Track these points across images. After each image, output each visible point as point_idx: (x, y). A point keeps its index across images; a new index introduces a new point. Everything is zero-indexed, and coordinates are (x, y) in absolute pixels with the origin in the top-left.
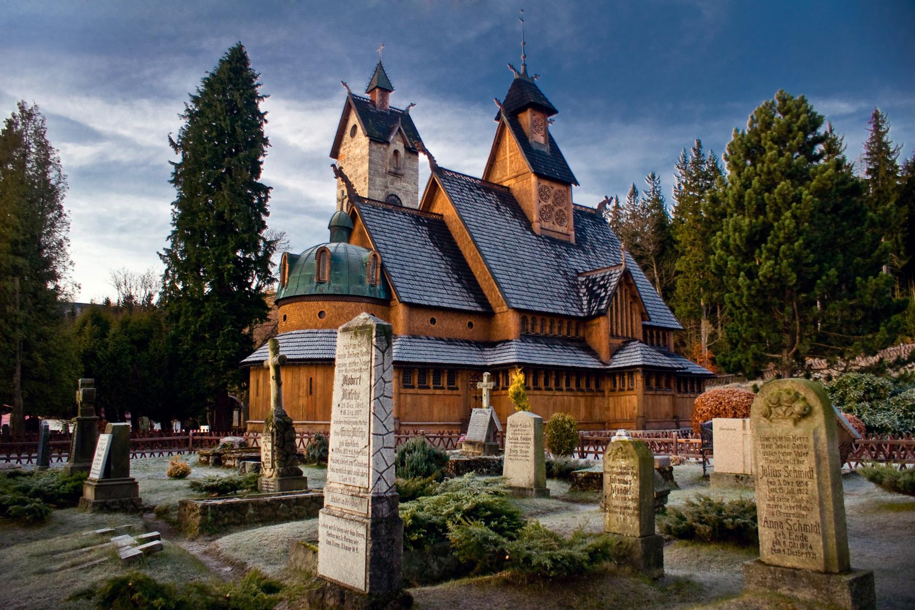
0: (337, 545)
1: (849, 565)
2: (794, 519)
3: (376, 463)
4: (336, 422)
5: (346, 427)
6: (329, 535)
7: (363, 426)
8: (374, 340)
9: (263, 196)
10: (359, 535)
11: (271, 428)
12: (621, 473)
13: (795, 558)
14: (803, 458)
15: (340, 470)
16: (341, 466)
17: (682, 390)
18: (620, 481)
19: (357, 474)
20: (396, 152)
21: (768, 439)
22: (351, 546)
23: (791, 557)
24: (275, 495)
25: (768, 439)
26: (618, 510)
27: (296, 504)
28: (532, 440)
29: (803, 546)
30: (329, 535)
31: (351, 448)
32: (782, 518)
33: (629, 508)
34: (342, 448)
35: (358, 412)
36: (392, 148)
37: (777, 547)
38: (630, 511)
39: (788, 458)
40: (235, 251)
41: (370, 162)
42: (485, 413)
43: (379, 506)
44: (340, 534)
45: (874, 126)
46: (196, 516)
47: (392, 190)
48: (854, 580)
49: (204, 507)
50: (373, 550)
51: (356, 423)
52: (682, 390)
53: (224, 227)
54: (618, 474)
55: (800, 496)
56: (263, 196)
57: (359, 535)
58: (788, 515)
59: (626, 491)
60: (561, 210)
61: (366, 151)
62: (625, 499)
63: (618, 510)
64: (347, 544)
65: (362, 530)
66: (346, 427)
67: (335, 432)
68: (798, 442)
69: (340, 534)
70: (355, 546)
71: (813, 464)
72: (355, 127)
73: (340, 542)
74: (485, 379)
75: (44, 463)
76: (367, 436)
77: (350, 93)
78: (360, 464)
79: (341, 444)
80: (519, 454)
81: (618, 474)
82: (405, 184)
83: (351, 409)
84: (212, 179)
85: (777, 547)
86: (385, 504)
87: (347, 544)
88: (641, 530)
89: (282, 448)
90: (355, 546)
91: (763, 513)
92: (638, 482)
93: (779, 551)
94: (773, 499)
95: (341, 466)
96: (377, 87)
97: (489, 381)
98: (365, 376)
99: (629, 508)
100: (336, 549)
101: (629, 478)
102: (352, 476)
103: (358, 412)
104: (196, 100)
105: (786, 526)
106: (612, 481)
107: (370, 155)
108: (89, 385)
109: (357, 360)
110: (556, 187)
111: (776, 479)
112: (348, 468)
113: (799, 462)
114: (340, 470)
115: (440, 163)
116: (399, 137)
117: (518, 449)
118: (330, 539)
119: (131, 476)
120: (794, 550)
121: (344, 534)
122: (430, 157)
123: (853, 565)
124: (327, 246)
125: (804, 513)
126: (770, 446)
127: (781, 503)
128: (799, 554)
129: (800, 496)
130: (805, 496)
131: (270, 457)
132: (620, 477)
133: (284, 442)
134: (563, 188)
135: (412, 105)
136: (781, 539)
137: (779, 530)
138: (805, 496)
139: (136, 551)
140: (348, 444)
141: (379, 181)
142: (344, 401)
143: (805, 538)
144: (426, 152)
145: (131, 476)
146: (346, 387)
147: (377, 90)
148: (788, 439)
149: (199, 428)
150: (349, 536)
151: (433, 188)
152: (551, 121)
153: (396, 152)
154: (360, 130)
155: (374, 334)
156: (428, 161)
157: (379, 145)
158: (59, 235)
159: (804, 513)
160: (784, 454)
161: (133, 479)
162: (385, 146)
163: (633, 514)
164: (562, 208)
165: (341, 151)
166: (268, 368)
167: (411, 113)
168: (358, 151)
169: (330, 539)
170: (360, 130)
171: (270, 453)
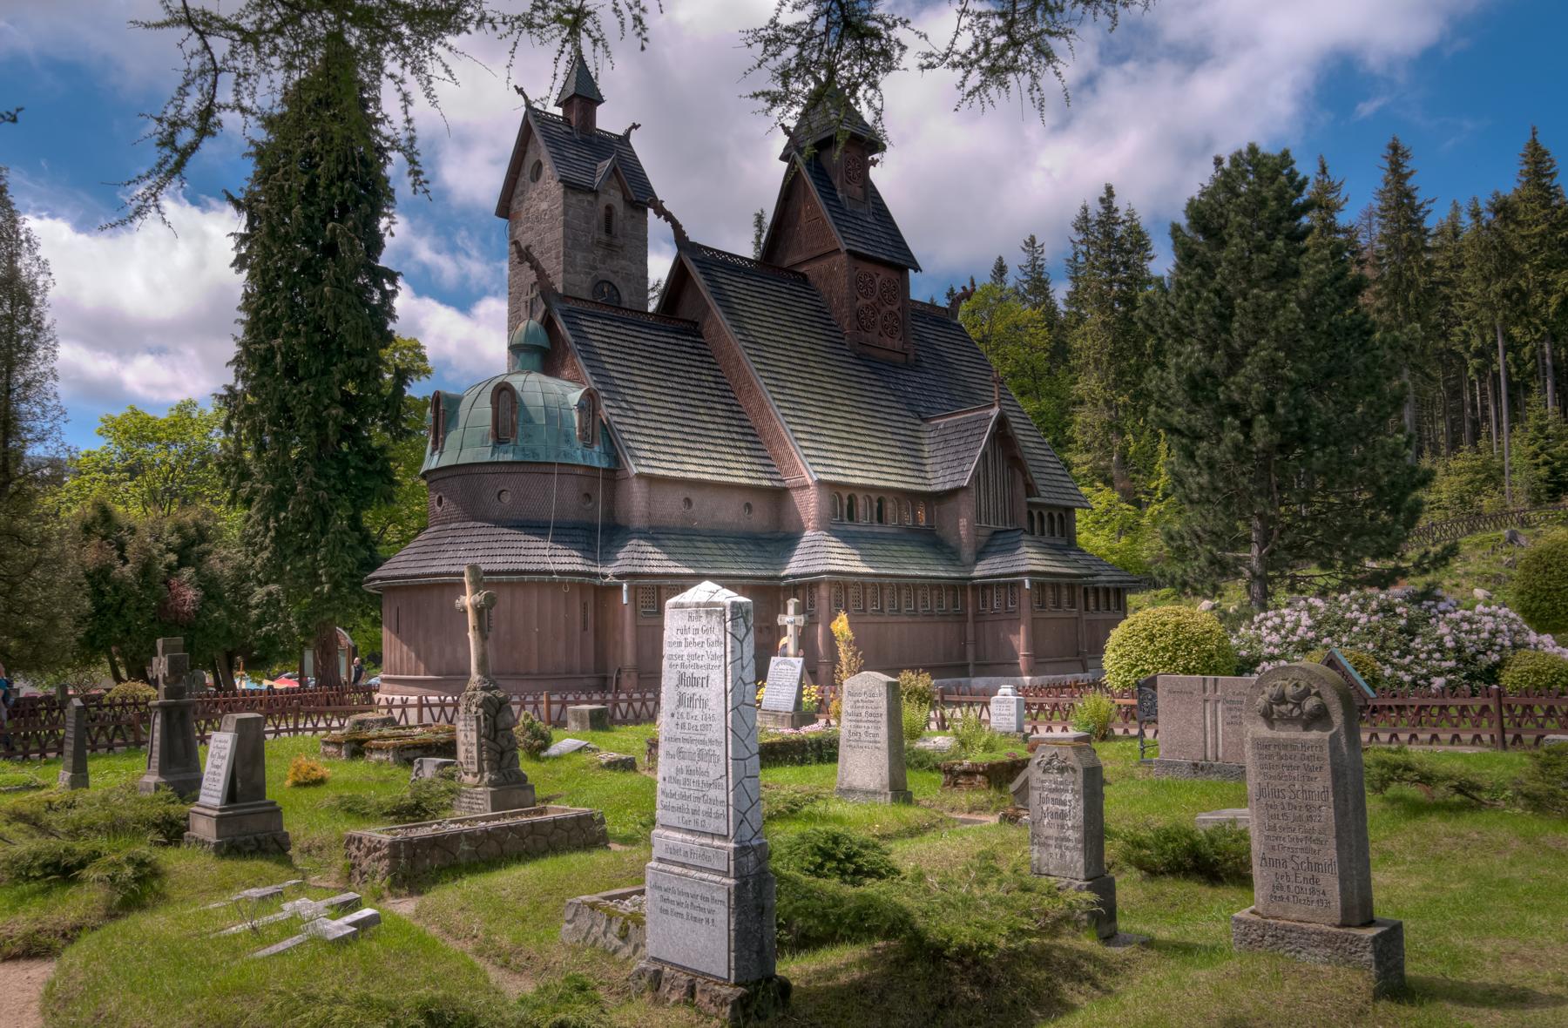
0: (679, 915)
1: (1372, 914)
2: (1303, 856)
3: (737, 800)
4: (669, 739)
5: (687, 746)
6: (666, 900)
7: (714, 747)
8: (729, 624)
9: (388, 287)
10: (714, 901)
11: (474, 709)
12: (1056, 790)
13: (1303, 907)
14: (1315, 774)
15: (680, 809)
16: (680, 803)
17: (1092, 607)
18: (1055, 802)
19: (708, 814)
20: (609, 208)
21: (1267, 747)
22: (702, 916)
23: (1298, 906)
24: (487, 819)
25: (1267, 747)
26: (1052, 842)
27: (532, 833)
28: (885, 718)
29: (1313, 891)
30: (666, 900)
31: (695, 778)
32: (1285, 855)
33: (1068, 840)
34: (681, 777)
35: (705, 727)
36: (604, 200)
37: (1278, 893)
38: (1071, 844)
39: (1296, 773)
40: (343, 383)
41: (566, 225)
42: (792, 664)
43: (744, 860)
44: (683, 899)
45: (1392, 162)
46: (379, 859)
47: (604, 273)
48: (1380, 935)
49: (394, 846)
50: (738, 923)
51: (703, 742)
52: (1092, 607)
53: (327, 347)
54: (1052, 791)
55: (1308, 826)
56: (388, 287)
57: (714, 901)
58: (1294, 850)
59: (1063, 815)
60: (891, 313)
61: (558, 210)
62: (1062, 827)
63: (1052, 842)
64: (695, 913)
65: (723, 896)
66: (687, 746)
67: (668, 753)
68: (1309, 753)
69: (683, 899)
70: (710, 917)
71: (1329, 783)
72: (539, 165)
73: (684, 911)
74: (791, 609)
75: (80, 778)
76: (723, 761)
77: (528, 104)
78: (714, 802)
79: (679, 771)
80: (863, 737)
81: (1052, 791)
82: (623, 262)
83: (693, 723)
84: (298, 264)
85: (1278, 893)
86: (751, 858)
87: (695, 913)
88: (1086, 871)
89: (494, 740)
90: (710, 917)
91: (1257, 847)
92: (1081, 802)
93: (1281, 898)
94: (1274, 828)
95: (680, 803)
96: (575, 95)
97: (797, 613)
98: (717, 677)
99: (1068, 840)
100: (677, 921)
101: (1069, 796)
102: (700, 818)
103: (705, 727)
104: (269, 122)
105: (1291, 865)
106: (1043, 800)
107: (565, 213)
108: (175, 649)
109: (700, 652)
110: (883, 275)
111: (1278, 801)
112: (692, 805)
113: (1310, 779)
114: (680, 809)
115: (694, 235)
116: (614, 182)
117: (862, 731)
118: (666, 906)
119: (269, 797)
120: (1301, 896)
121: (689, 900)
122: (676, 227)
123: (1377, 915)
124: (508, 380)
125: (1314, 846)
126: (1271, 756)
127: (1284, 834)
128: (1308, 901)
129: (1308, 826)
130: (1317, 825)
131: (475, 754)
132: (1054, 796)
133: (496, 731)
134: (894, 276)
135: (635, 126)
136: (1284, 882)
137: (1281, 871)
138: (1317, 825)
139: (339, 927)
140: (690, 772)
141: (579, 257)
142: (681, 710)
143: (1315, 881)
144: (661, 211)
145: (269, 797)
146: (683, 689)
147: (576, 101)
148: (1294, 748)
149: (164, 654)
150: (699, 902)
151: (679, 273)
152: (874, 163)
153: (609, 208)
154: (548, 169)
155: (728, 616)
156: (671, 232)
157: (581, 197)
158: (37, 366)
159: (1314, 846)
160: (1289, 767)
161: (273, 803)
162: (590, 198)
163: (1075, 848)
164: (895, 308)
165: (515, 205)
166: (465, 612)
167: (632, 141)
168: (544, 206)
169: (666, 906)
170: (548, 169)
171: (475, 749)
